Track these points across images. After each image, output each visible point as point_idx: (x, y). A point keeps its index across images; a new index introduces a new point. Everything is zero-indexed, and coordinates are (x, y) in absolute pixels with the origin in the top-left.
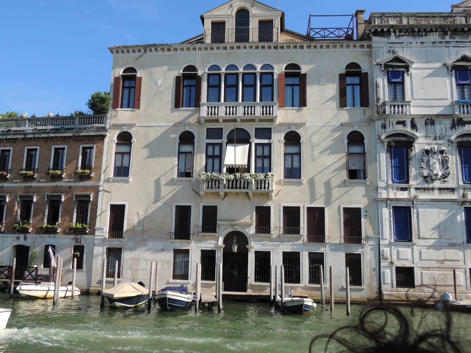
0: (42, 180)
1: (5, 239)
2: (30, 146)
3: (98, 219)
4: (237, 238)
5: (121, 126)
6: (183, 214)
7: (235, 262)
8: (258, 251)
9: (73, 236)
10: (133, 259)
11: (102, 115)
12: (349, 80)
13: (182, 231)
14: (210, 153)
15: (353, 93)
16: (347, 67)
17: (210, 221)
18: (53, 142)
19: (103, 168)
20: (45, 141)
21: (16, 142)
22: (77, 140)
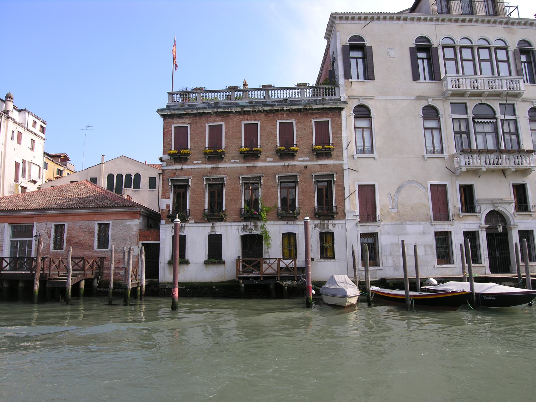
0: (268, 159)
1: (229, 228)
2: (247, 120)
3: (347, 201)
4: (495, 216)
5: (358, 98)
6: (439, 193)
7: (498, 241)
8: (468, 232)
9: (211, 224)
10: (392, 244)
11: (333, 86)
12: (353, 54)
13: (441, 211)
14: (457, 129)
15: (423, 66)
16: (351, 39)
17: (469, 202)
18: (277, 115)
19: (344, 145)
20: (266, 115)
21: (228, 116)
22: (308, 114)
